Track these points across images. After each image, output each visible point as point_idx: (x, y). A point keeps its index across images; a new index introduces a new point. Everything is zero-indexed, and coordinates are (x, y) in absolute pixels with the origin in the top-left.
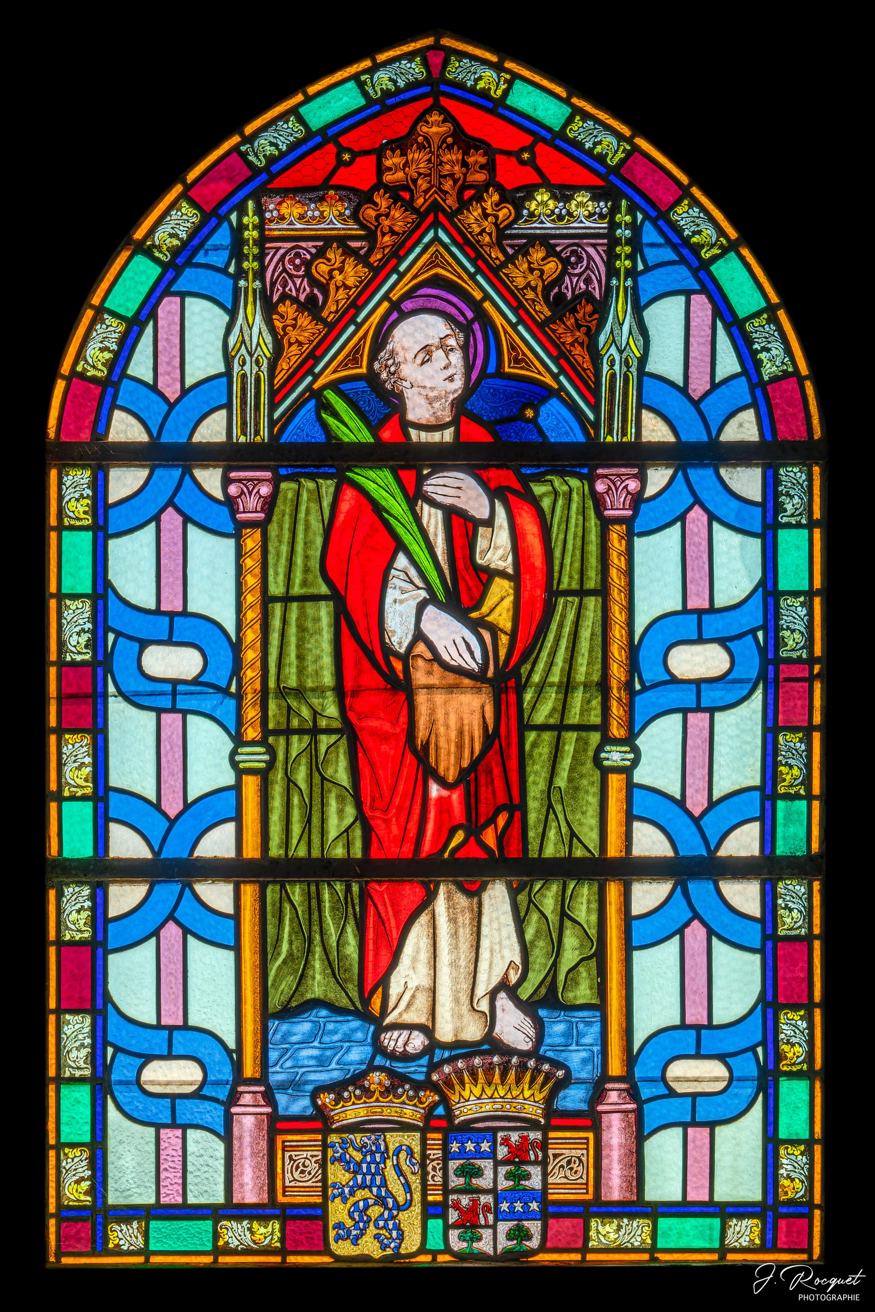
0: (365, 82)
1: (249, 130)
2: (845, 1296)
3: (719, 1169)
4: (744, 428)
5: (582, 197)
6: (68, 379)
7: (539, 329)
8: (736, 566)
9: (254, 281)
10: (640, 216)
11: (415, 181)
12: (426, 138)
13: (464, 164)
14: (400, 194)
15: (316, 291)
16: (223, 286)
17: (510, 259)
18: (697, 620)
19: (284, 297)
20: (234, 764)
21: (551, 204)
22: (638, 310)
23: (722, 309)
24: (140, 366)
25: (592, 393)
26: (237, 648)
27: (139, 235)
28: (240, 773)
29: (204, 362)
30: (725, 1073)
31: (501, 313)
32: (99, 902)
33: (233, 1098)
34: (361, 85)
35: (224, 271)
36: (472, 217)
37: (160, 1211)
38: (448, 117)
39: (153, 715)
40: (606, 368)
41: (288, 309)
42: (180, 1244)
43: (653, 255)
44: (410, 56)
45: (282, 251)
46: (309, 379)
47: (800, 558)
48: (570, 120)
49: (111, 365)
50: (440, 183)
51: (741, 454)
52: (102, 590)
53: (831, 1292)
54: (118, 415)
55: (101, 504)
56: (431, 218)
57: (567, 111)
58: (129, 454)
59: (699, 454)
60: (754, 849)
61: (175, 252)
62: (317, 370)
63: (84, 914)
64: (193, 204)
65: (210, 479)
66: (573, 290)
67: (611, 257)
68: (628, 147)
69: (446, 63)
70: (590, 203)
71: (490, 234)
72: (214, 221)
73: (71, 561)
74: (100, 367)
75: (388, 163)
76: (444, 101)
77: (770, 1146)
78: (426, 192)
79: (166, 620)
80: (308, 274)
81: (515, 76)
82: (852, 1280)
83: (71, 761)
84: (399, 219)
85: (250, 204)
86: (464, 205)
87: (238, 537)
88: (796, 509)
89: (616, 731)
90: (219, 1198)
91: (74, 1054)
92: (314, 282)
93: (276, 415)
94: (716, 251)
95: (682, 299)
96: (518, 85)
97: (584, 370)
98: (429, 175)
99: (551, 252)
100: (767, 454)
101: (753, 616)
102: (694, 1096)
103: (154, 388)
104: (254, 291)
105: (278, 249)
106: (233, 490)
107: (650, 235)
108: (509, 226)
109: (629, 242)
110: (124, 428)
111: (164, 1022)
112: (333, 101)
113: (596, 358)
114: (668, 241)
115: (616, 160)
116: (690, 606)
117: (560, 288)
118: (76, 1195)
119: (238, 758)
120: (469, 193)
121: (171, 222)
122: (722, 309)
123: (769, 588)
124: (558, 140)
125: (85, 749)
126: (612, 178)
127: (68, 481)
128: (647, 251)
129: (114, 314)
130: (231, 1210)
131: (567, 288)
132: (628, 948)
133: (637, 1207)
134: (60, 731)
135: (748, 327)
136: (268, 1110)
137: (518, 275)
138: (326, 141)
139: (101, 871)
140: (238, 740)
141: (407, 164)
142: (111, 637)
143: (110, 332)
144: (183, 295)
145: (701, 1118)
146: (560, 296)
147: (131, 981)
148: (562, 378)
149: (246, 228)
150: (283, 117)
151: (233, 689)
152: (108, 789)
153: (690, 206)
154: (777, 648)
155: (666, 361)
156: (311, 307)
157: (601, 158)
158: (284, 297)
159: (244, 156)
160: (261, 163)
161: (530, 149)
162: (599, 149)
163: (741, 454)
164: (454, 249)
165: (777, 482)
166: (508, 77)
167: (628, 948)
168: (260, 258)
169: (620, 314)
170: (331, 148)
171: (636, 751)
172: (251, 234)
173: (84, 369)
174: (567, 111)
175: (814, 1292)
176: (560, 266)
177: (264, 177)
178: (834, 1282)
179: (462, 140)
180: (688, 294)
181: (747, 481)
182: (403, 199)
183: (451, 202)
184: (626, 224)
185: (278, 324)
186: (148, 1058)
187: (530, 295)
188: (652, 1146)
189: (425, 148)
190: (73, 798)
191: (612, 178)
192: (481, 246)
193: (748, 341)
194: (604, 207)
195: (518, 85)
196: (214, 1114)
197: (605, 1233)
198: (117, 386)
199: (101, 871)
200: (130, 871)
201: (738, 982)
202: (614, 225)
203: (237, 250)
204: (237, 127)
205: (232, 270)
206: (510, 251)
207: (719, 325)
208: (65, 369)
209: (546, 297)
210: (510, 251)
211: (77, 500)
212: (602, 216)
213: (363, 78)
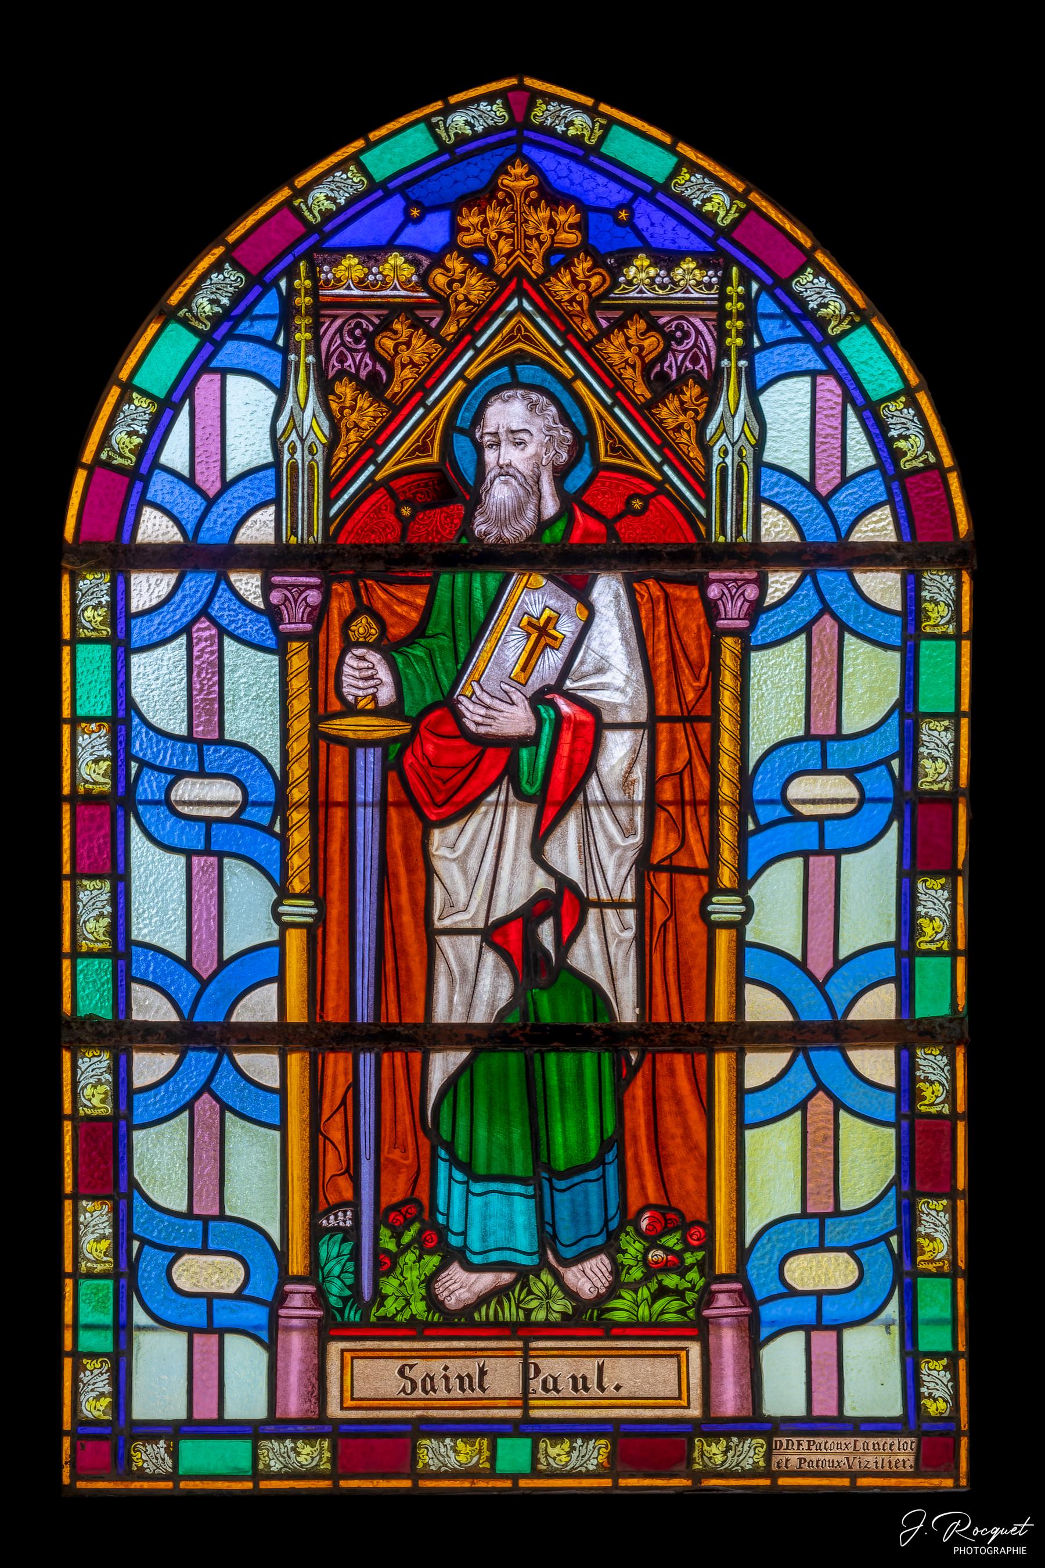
0: (437, 125)
1: (301, 181)
2: (1009, 1549)
3: (854, 1378)
4: (879, 527)
5: (689, 264)
6: (90, 468)
7: (644, 414)
8: (870, 682)
9: (307, 354)
10: (755, 286)
11: (495, 244)
12: (509, 195)
13: (552, 223)
14: (479, 258)
15: (378, 367)
16: (271, 362)
17: (605, 334)
18: (820, 743)
19: (341, 374)
20: (277, 916)
21: (652, 272)
22: (754, 394)
23: (855, 395)
24: (175, 453)
25: (701, 487)
26: (282, 784)
27: (175, 299)
28: (284, 927)
29: (248, 445)
30: (854, 793)
31: (593, 393)
32: (121, 1072)
33: (281, 1298)
34: (432, 128)
35: (272, 344)
36: (561, 287)
37: (191, 1428)
38: (534, 169)
39: (182, 1338)
40: (716, 460)
41: (345, 389)
42: (213, 1462)
43: (771, 329)
44: (490, 98)
45: (338, 322)
46: (371, 468)
47: (946, 675)
48: (676, 172)
49: (140, 452)
50: (526, 248)
51: (876, 556)
52: (123, 713)
53: (992, 1544)
54: (148, 512)
55: (123, 1089)
56: (513, 285)
57: (672, 161)
58: (157, 557)
59: (828, 556)
60: (889, 1013)
61: (216, 320)
62: (380, 459)
63: (105, 922)
64: (237, 266)
65: (248, 584)
66: (679, 369)
67: (722, 333)
68: (743, 206)
69: (532, 105)
70: (697, 272)
71: (580, 304)
72: (257, 290)
73: (86, 679)
74: (128, 454)
75: (465, 223)
76: (526, 149)
77: (909, 1359)
78: (508, 256)
79: (199, 1224)
80: (370, 348)
81: (612, 121)
82: (1017, 1530)
83: (88, 907)
84: (476, 287)
85: (302, 266)
86: (551, 271)
87: (281, 651)
88: (710, 1458)
89: (726, 877)
90: (258, 1410)
91: (91, 925)
92: (376, 357)
93: (333, 512)
94: (845, 326)
95: (799, 861)
96: (616, 129)
97: (690, 459)
98: (512, 236)
99: (653, 326)
100: (909, 557)
101: (890, 741)
102: (820, 819)
103: (190, 481)
104: (307, 365)
105: (335, 318)
106: (276, 597)
107: (766, 305)
108: (605, 295)
109: (741, 315)
110: (154, 528)
111: (196, 1211)
112: (401, 148)
113: (706, 450)
114: (787, 312)
115: (727, 222)
116: (810, 1210)
117: (662, 367)
118: (94, 775)
119: (281, 909)
120: (555, 259)
121: (210, 286)
122: (855, 395)
123: (908, 711)
124: (656, 193)
125: (105, 1376)
126: (722, 242)
127: (83, 1064)
128: (760, 810)
129: (144, 393)
130: (273, 1427)
131: (670, 367)
132: (741, 1126)
133: (755, 1423)
134: (75, 877)
135: (883, 412)
136: (318, 1313)
137: (614, 350)
138: (388, 195)
139: (122, 1036)
140: (283, 892)
141: (485, 224)
142: (136, 1244)
143: (140, 408)
144: (224, 372)
145: (824, 1321)
146: (663, 376)
147: (159, 1161)
148: (666, 468)
149: (297, 292)
150: (342, 166)
151: (277, 828)
152: (129, 943)
153: (816, 276)
154: (915, 778)
155: (788, 446)
156: (373, 386)
157: (710, 219)
158: (341, 374)
159: (297, 212)
160: (314, 218)
161: (628, 206)
162: (708, 207)
163: (876, 556)
164: (539, 320)
165: (913, 1066)
166: (604, 122)
167: (741, 1126)
168: (315, 328)
169: (732, 403)
170: (397, 203)
171: (748, 903)
172: (304, 301)
173: (109, 457)
174: (672, 161)
175: (972, 1544)
176: (662, 345)
177: (315, 238)
178: (996, 1532)
179: (550, 195)
180: (814, 374)
181: (883, 586)
182: (479, 263)
183: (537, 268)
184: (737, 331)
185: (334, 406)
186: (179, 775)
187: (628, 373)
188: (767, 1354)
189: (507, 205)
190: (91, 1275)
191: (722, 242)
192: (571, 316)
193: (883, 427)
194: (711, 276)
195: (616, 129)
196: (258, 1315)
197: (715, 1452)
198: (146, 480)
199: (122, 1036)
200: (154, 1036)
201: (868, 1157)
202: (724, 298)
203: (286, 316)
204: (286, 177)
205: (280, 342)
206: (604, 324)
207: (850, 412)
208: (88, 457)
209: (646, 369)
210: (604, 324)
211: (95, 1087)
212: (709, 286)
213: (434, 120)
